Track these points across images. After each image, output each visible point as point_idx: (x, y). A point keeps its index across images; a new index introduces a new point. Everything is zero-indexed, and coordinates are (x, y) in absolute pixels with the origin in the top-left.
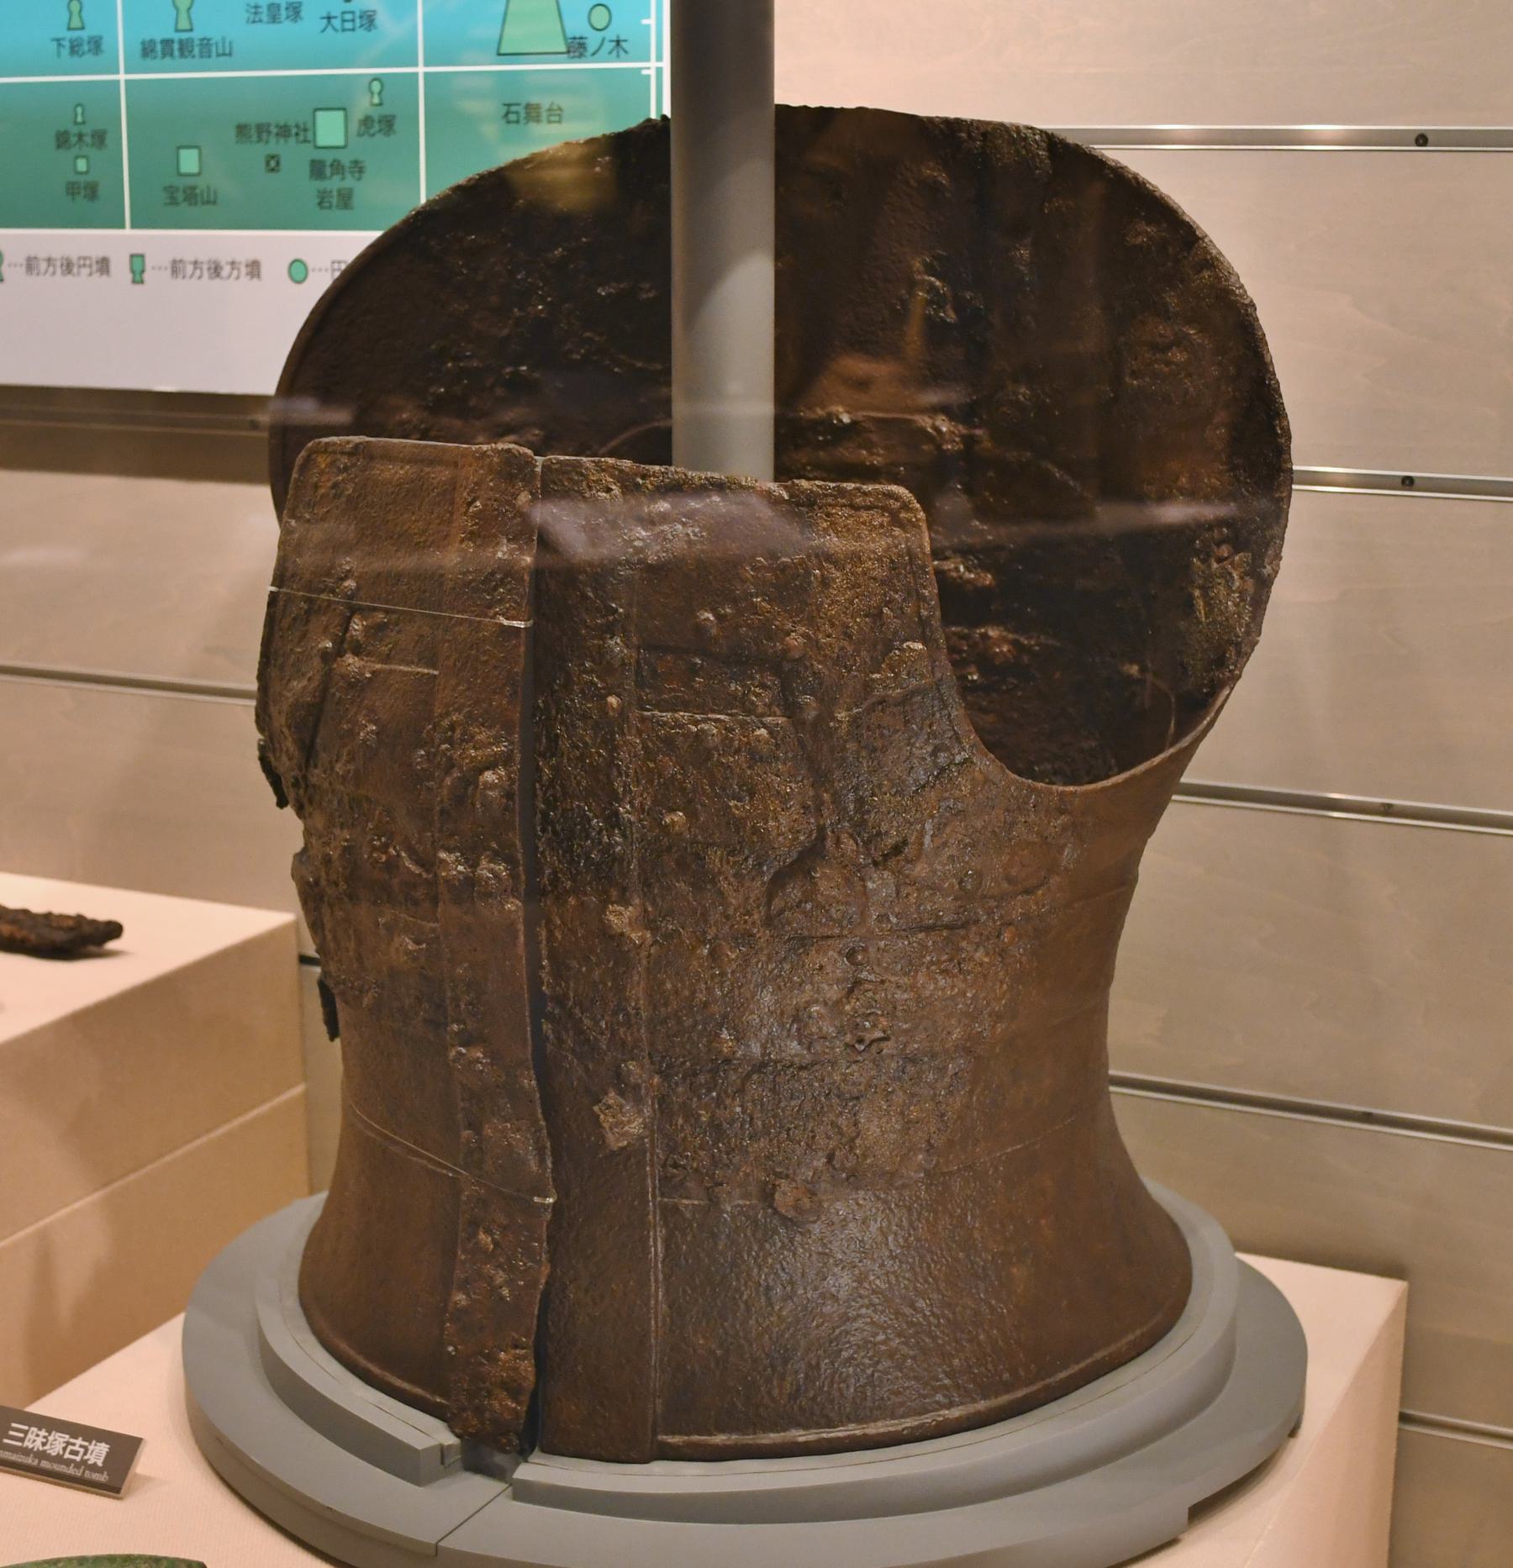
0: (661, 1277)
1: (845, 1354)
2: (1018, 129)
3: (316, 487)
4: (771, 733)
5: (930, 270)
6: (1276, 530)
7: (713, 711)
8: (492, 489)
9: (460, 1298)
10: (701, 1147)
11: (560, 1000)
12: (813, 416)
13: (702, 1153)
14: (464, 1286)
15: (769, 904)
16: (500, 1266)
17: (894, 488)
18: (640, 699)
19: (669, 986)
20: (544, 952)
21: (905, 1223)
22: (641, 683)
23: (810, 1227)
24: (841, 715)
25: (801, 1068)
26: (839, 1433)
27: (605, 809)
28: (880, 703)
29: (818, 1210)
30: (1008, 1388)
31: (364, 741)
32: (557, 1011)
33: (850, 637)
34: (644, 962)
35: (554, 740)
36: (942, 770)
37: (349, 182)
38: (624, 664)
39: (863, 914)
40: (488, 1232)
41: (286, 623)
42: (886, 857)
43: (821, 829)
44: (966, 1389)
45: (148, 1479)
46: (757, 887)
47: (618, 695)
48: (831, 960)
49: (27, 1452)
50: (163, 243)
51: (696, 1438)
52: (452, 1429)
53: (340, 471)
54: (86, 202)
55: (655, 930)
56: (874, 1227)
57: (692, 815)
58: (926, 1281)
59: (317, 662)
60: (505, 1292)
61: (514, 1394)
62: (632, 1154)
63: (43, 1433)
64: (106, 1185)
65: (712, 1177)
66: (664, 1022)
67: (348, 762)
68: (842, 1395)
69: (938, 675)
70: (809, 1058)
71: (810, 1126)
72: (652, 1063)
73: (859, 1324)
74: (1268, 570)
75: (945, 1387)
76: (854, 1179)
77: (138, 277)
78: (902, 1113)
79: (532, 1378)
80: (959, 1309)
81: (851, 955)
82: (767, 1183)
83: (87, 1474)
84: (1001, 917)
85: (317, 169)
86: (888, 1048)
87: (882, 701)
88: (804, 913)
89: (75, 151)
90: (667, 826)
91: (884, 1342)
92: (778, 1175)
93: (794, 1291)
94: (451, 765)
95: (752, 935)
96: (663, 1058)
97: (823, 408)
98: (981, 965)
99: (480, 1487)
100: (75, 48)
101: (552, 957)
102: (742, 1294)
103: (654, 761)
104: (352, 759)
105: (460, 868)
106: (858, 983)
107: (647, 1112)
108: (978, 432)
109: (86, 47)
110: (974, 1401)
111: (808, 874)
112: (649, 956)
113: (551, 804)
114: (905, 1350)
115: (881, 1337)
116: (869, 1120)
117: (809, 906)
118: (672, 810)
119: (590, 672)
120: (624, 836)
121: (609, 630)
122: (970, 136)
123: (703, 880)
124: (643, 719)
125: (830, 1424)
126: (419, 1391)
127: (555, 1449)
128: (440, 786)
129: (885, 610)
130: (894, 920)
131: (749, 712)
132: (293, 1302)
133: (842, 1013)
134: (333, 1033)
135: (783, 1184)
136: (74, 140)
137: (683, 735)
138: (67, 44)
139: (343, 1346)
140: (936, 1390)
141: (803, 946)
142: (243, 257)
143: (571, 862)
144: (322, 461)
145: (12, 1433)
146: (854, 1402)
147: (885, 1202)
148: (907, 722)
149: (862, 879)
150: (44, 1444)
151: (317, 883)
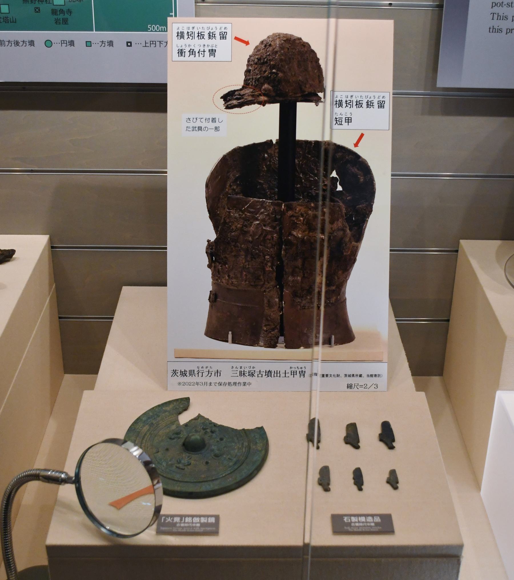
37: (66, 16)
85: (54, 12)
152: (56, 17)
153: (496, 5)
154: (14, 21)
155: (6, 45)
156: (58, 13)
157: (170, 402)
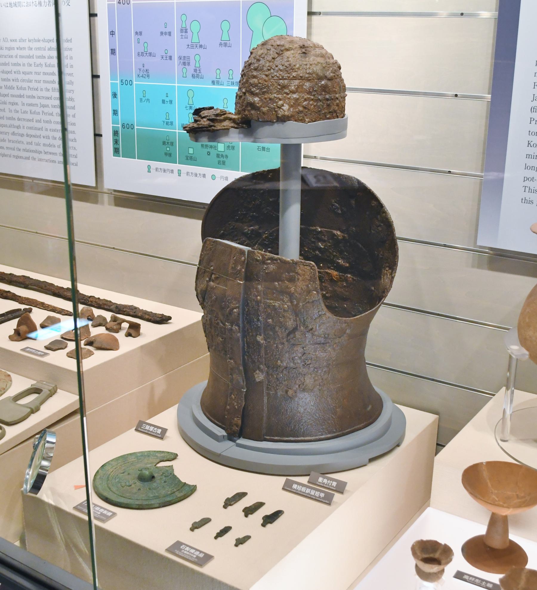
5: (336, 202)
6: (395, 267)
9: (228, 407)
11: (248, 352)
17: (311, 262)
26: (299, 439)
29: (296, 396)
30: (334, 432)
35: (248, 303)
41: (200, 273)
42: (310, 330)
43: (297, 325)
45: (168, 437)
46: (285, 335)
48: (299, 349)
49: (146, 430)
54: (169, 157)
56: (308, 400)
57: (273, 320)
70: (295, 367)
76: (304, 390)
79: (527, 353)
81: (303, 348)
85: (218, 156)
86: (311, 366)
89: (167, 146)
99: (231, 443)
100: (167, 123)
101: (247, 343)
104: (211, 302)
106: (305, 353)
109: (170, 124)
111: (295, 332)
118: (269, 319)
123: (275, 332)
125: (298, 437)
126: (220, 424)
127: (244, 438)
132: (199, 404)
139: (207, 414)
140: (319, 432)
144: (208, 242)
148: (313, 306)
152: (219, 159)
153: (528, 179)
157: (163, 452)
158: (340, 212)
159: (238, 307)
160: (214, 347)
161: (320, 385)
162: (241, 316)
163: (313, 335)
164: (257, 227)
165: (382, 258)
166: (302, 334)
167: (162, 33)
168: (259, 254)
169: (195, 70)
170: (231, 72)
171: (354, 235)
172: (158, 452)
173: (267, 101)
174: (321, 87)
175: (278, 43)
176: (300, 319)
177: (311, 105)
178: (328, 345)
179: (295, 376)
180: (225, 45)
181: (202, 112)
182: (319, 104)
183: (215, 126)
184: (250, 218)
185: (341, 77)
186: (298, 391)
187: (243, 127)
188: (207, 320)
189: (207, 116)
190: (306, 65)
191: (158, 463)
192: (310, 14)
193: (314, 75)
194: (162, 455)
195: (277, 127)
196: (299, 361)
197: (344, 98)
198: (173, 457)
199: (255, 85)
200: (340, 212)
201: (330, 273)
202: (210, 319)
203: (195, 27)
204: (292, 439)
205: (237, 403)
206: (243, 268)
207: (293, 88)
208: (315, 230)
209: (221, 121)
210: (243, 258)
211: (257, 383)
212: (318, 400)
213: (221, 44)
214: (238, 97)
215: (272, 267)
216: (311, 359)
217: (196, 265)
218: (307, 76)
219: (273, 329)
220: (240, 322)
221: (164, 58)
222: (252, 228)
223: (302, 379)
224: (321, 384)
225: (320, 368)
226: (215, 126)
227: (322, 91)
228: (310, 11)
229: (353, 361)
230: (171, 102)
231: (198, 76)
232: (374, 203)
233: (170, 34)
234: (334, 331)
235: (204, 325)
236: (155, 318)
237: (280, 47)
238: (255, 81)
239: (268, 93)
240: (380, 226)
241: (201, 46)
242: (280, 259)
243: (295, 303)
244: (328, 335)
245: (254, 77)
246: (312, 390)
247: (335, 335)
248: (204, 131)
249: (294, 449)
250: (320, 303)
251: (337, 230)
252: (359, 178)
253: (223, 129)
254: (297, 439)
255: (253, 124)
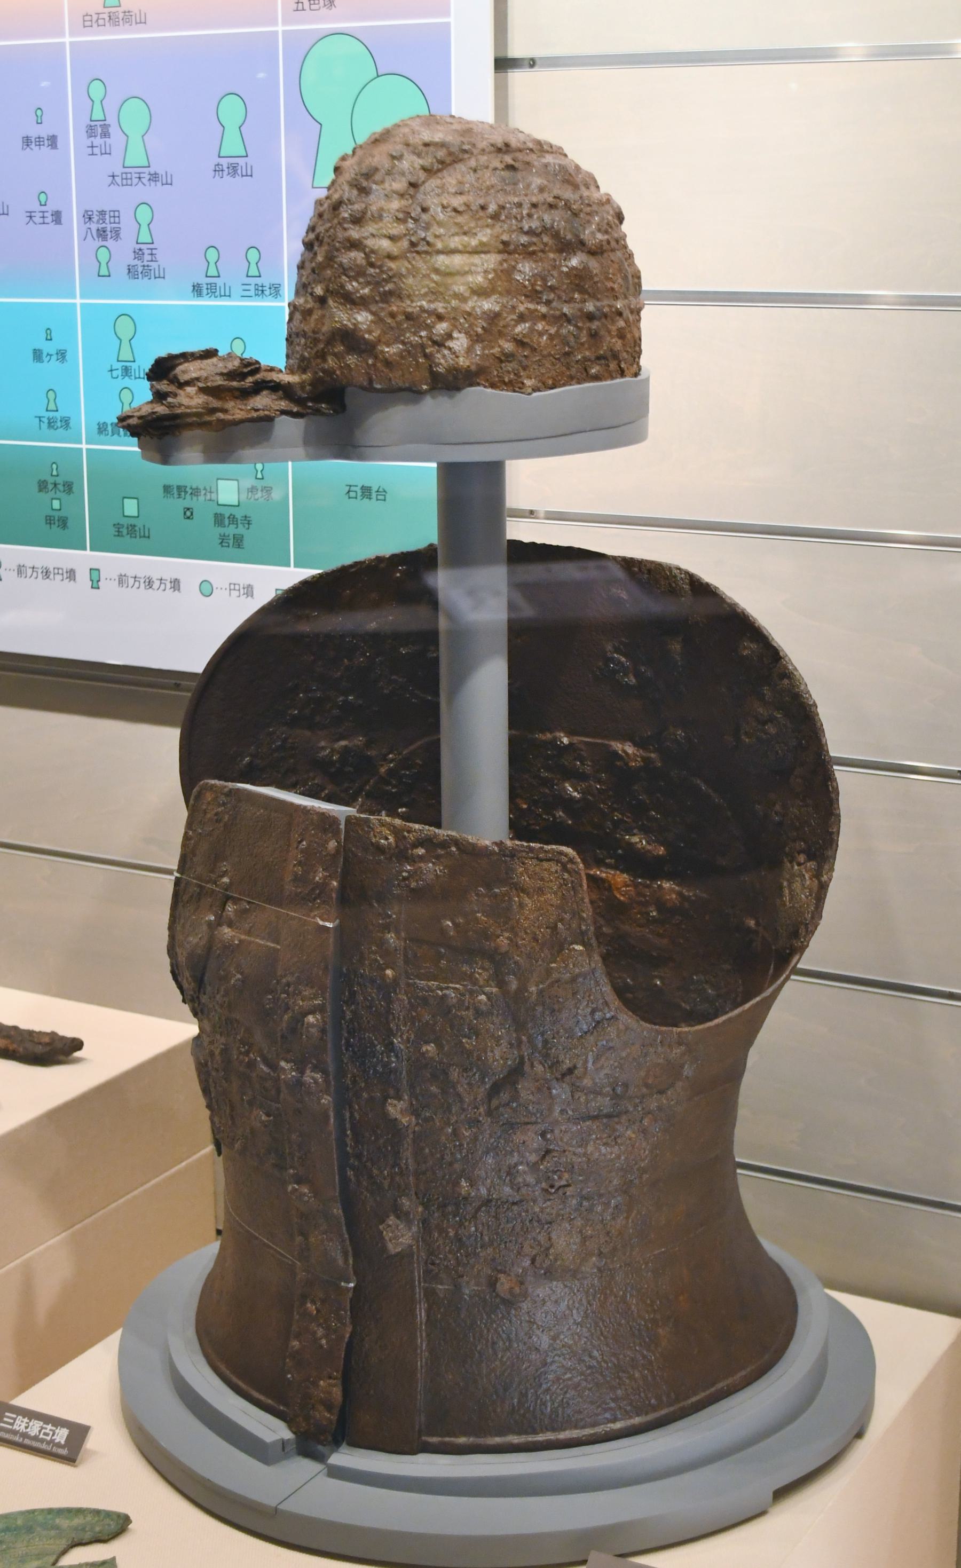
0: (424, 1334)
1: (544, 1386)
2: (670, 568)
3: (205, 812)
4: (489, 998)
5: (617, 650)
6: (830, 853)
7: (452, 983)
8: (313, 835)
9: (295, 1344)
10: (450, 1252)
11: (359, 1156)
12: (544, 738)
13: (450, 1256)
14: (297, 1337)
15: (490, 1101)
16: (320, 1325)
18: (406, 972)
19: (427, 1151)
20: (348, 1126)
21: (584, 1301)
22: (407, 961)
23: (521, 1305)
24: (533, 989)
25: (514, 1204)
26: (540, 1438)
27: (384, 1040)
28: (557, 982)
29: (525, 1295)
30: (654, 1409)
31: (234, 985)
32: (356, 1163)
33: (537, 941)
34: (411, 1136)
35: (353, 994)
36: (598, 1022)
37: (241, 530)
38: (396, 950)
39: (550, 1110)
40: (313, 1302)
41: (186, 898)
42: (564, 1075)
43: (522, 1058)
44: (626, 1411)
45: (93, 1453)
46: (482, 1092)
47: (393, 969)
49: (15, 1432)
50: (114, 562)
51: (447, 1439)
52: (290, 1428)
53: (219, 805)
54: (58, 529)
55: (418, 1116)
56: (563, 1305)
57: (440, 1046)
58: (599, 1339)
59: (205, 928)
60: (324, 1341)
61: (329, 1408)
62: (406, 1256)
63: (26, 1420)
64: (69, 1228)
65: (456, 1272)
66: (424, 1173)
67: (223, 996)
68: (542, 1412)
69: (593, 965)
70: (517, 1198)
71: (520, 1240)
72: (418, 1198)
73: (553, 1367)
74: (825, 878)
75: (611, 1409)
76: (549, 1274)
77: (95, 584)
78: (581, 1232)
80: (621, 1356)
81: (543, 1134)
82: (491, 1276)
83: (55, 1450)
84: (643, 1109)
85: (219, 520)
86: (569, 1191)
87: (558, 981)
88: (512, 1108)
89: (52, 494)
90: (423, 1054)
91: (570, 1379)
92: (500, 1272)
93: (510, 1346)
94: (287, 1008)
95: (479, 1121)
96: (425, 1195)
97: (551, 733)
98: (630, 1139)
99: (305, 1467)
102: (476, 1347)
103: (416, 1012)
104: (226, 994)
105: (294, 1073)
106: (548, 1152)
107: (414, 1229)
108: (653, 755)
109: (59, 424)
110: (631, 1417)
111: (515, 1083)
112: (414, 1132)
113: (351, 1033)
114: (584, 1384)
115: (568, 1376)
116: (559, 1237)
117: (514, 1105)
118: (427, 1043)
119: (375, 953)
120: (397, 1056)
121: (386, 928)
122: (640, 570)
124: (408, 985)
125: (535, 1432)
128: (281, 1020)
129: (560, 925)
130: (570, 1112)
131: (474, 984)
133: (539, 1169)
134: (219, 1154)
135: (502, 1277)
136: (50, 487)
137: (433, 996)
138: (46, 421)
139: (223, 1368)
140: (606, 1410)
141: (512, 1128)
142: (168, 576)
143: (364, 1071)
144: (209, 796)
145: (5, 1419)
146: (550, 1417)
147: (571, 1288)
148: (574, 994)
149: (549, 1089)
150: (26, 1428)
151: (206, 1064)
152: (221, 530)
154: (147, 535)
155: (130, 585)
156: (227, 522)
157: (79, 1511)
158: (632, 680)
159: (321, 1009)
160: (237, 1145)
161: (600, 1254)
162: (329, 1037)
163: (575, 1088)
164: (360, 740)
165: (780, 824)
166: (539, 1090)
167: (27, 141)
168: (385, 827)
169: (138, 254)
170: (253, 255)
171: (687, 754)
172: (60, 1512)
173: (399, 324)
174: (567, 275)
175: (426, 136)
176: (530, 1038)
177: (541, 334)
178: (624, 1118)
179: (518, 1228)
180: (234, 170)
181: (181, 368)
182: (564, 331)
183: (225, 411)
184: (336, 712)
185: (625, 247)
186: (530, 1278)
187: (317, 412)
188: (212, 1054)
189: (198, 379)
190: (519, 205)
191: (64, 1552)
192: (503, 64)
193: (546, 239)
194: (77, 1521)
195: (434, 408)
196: (530, 1179)
197: (637, 312)
198: (113, 1526)
199: (359, 273)
200: (632, 680)
201: (603, 880)
202: (225, 1051)
203: (133, 118)
204: (515, 1439)
205: (328, 1328)
206: (331, 877)
207: (480, 279)
208: (553, 743)
209: (245, 394)
210: (332, 844)
211: (390, 1257)
212: (595, 1305)
213: (218, 170)
214: (298, 316)
215: (431, 869)
216: (571, 1170)
217: (169, 872)
218: (524, 239)
219: (440, 1075)
220: (329, 1059)
221: (37, 219)
222: (343, 743)
223: (542, 1238)
224: (605, 1250)
225: (601, 1196)
226: (225, 411)
227: (573, 291)
228: (501, 55)
229: (701, 1168)
230: (62, 355)
231: (147, 272)
232: (748, 648)
233: (53, 141)
234: (643, 1074)
235: (203, 1070)
236: (29, 1046)
237: (432, 148)
238: (357, 256)
239: (400, 297)
240: (771, 720)
241: (154, 177)
242: (456, 842)
243: (514, 986)
244: (626, 1086)
245: (355, 245)
246: (575, 1274)
247: (647, 1085)
248: (191, 426)
249: (530, 1476)
250: (597, 983)
251: (623, 738)
252: (693, 570)
253: (252, 420)
254: (530, 1438)
255: (353, 399)
